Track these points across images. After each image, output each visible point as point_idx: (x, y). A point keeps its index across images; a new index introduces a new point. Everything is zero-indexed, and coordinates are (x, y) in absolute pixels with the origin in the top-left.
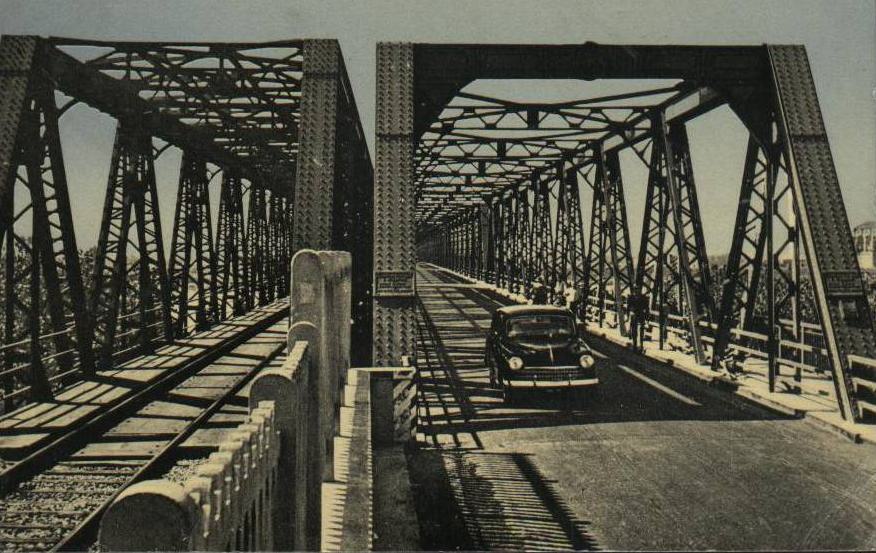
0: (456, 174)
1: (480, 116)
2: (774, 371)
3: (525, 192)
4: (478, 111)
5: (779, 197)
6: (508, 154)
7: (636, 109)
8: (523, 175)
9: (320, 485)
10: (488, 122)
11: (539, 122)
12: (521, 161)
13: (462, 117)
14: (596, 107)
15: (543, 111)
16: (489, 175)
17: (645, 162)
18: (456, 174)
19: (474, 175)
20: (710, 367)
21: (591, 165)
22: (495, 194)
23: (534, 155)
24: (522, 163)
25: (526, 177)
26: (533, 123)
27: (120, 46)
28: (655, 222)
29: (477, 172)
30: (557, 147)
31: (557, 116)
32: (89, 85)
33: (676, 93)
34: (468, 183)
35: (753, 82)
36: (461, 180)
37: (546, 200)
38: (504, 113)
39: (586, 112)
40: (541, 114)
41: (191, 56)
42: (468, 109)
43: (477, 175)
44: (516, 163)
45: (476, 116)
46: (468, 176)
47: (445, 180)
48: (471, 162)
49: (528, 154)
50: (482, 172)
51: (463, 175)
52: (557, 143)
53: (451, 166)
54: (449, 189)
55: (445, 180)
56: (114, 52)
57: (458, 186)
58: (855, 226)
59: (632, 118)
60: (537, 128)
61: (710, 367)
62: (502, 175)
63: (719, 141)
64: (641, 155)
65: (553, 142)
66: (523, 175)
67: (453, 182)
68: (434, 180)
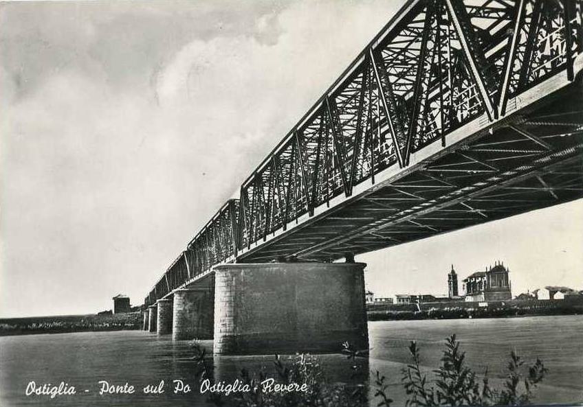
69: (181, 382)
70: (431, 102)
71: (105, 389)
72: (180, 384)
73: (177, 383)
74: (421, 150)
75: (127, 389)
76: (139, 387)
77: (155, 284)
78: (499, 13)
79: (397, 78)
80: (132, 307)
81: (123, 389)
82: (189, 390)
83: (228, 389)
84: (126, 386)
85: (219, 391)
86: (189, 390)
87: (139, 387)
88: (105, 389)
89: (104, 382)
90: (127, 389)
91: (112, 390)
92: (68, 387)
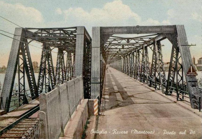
0: (116, 48)
1: (117, 40)
2: (178, 96)
3: (133, 53)
4: (116, 40)
5: (179, 59)
6: (124, 48)
7: (150, 38)
8: (133, 48)
9: (59, 30)
10: (119, 42)
11: (129, 41)
12: (133, 44)
13: (113, 41)
14: (141, 38)
15: (127, 40)
16: (121, 51)
17: (152, 50)
18: (116, 48)
19: (121, 48)
20: (165, 94)
21: (141, 50)
22: (126, 53)
23: (137, 43)
24: (133, 45)
25: (134, 49)
26: (128, 41)
27: (39, 29)
28: (174, 57)
29: (122, 48)
30: (143, 41)
31: (133, 40)
32: (34, 36)
33: (157, 35)
34: (120, 51)
35: (173, 33)
36: (120, 47)
37: (139, 54)
38: (122, 40)
39: (140, 39)
40: (130, 40)
41: (54, 31)
42: (114, 39)
43: (122, 49)
44: (132, 45)
45: (116, 40)
46: (120, 49)
47: (114, 50)
48: (120, 45)
49: (135, 42)
50: (120, 51)
51: (118, 48)
52: (135, 45)
53: (118, 41)
54: (115, 52)
55: (114, 50)
56: (38, 31)
57: (117, 51)
58: (167, 72)
59: (149, 40)
60: (129, 43)
61: (165, 94)
62: (128, 48)
63: (167, 45)
64: (151, 48)
65: (142, 39)
66: (133, 48)
67: (116, 50)
68: (112, 50)
69: (192, 130)
70: (172, 42)
71: (165, 133)
72: (166, 131)
73: (191, 131)
74: (21, 111)
75: (173, 133)
76: (178, 132)
77: (30, 52)
78: (48, 65)
79: (28, 58)
80: (6, 66)
81: (172, 133)
82: (195, 133)
83: (100, 132)
84: (144, 131)
85: (144, 133)
86: (195, 133)
87: (178, 132)
88: (165, 133)
89: (165, 130)
90: (173, 133)
91: (168, 133)
92: (105, 131)
